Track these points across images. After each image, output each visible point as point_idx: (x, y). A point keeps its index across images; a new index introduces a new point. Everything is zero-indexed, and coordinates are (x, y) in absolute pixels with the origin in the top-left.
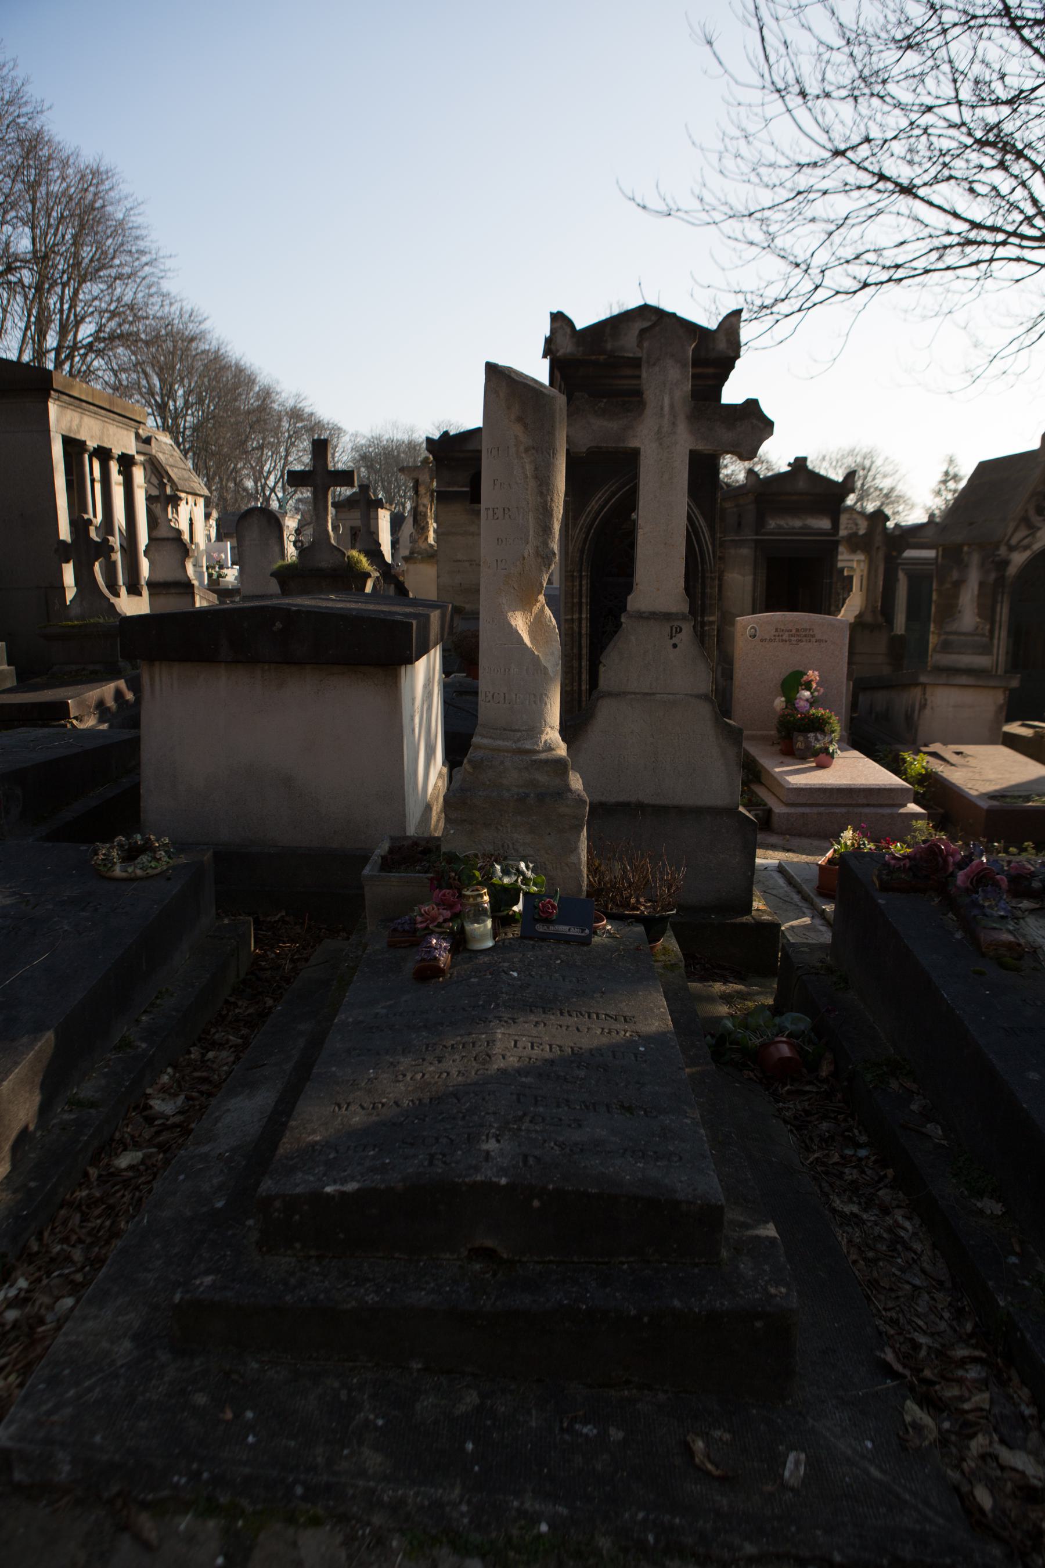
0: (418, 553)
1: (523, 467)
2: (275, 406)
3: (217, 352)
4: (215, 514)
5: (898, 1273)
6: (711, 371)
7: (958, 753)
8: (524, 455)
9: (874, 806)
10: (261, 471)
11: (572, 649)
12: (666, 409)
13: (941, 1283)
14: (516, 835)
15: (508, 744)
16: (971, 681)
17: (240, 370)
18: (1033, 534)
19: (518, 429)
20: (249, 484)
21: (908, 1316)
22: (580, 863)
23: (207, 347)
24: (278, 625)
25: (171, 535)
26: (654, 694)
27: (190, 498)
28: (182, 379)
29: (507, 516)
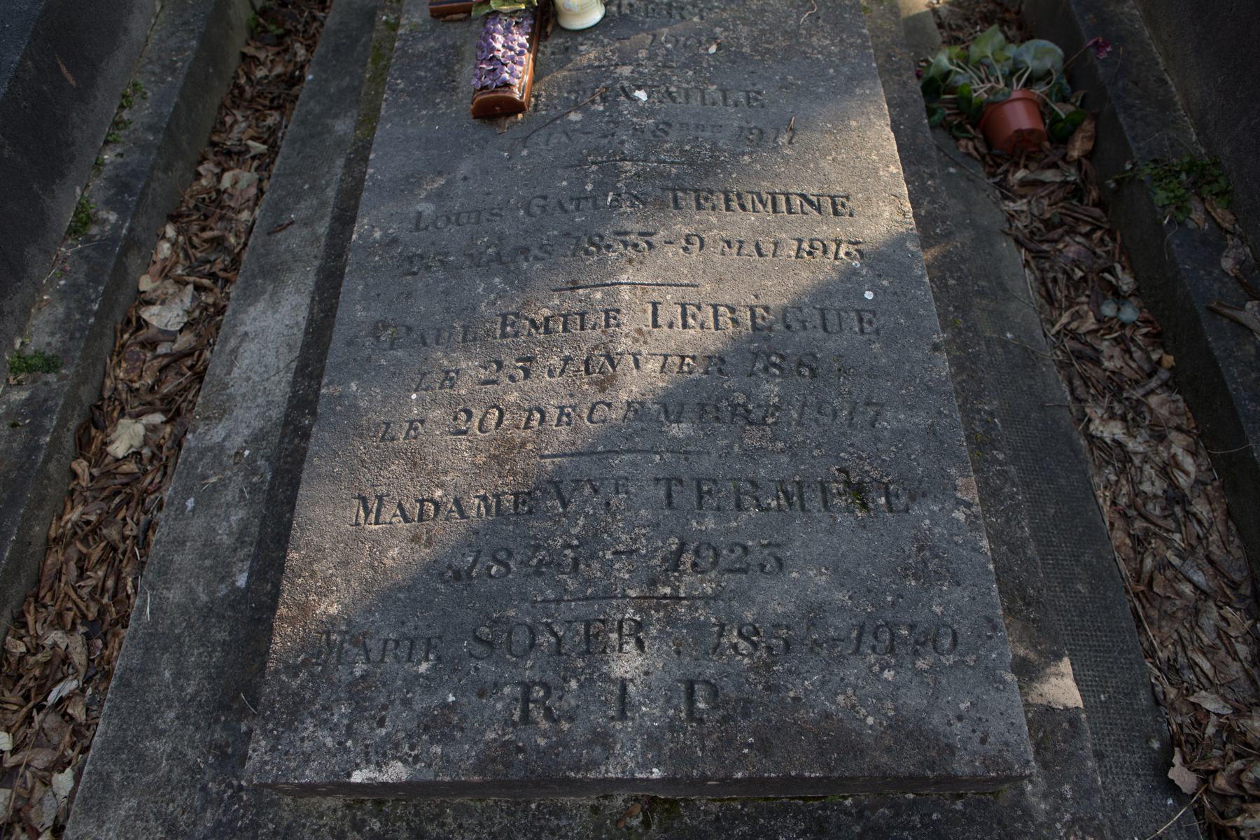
5: (1176, 561)
13: (1234, 586)
21: (1190, 654)
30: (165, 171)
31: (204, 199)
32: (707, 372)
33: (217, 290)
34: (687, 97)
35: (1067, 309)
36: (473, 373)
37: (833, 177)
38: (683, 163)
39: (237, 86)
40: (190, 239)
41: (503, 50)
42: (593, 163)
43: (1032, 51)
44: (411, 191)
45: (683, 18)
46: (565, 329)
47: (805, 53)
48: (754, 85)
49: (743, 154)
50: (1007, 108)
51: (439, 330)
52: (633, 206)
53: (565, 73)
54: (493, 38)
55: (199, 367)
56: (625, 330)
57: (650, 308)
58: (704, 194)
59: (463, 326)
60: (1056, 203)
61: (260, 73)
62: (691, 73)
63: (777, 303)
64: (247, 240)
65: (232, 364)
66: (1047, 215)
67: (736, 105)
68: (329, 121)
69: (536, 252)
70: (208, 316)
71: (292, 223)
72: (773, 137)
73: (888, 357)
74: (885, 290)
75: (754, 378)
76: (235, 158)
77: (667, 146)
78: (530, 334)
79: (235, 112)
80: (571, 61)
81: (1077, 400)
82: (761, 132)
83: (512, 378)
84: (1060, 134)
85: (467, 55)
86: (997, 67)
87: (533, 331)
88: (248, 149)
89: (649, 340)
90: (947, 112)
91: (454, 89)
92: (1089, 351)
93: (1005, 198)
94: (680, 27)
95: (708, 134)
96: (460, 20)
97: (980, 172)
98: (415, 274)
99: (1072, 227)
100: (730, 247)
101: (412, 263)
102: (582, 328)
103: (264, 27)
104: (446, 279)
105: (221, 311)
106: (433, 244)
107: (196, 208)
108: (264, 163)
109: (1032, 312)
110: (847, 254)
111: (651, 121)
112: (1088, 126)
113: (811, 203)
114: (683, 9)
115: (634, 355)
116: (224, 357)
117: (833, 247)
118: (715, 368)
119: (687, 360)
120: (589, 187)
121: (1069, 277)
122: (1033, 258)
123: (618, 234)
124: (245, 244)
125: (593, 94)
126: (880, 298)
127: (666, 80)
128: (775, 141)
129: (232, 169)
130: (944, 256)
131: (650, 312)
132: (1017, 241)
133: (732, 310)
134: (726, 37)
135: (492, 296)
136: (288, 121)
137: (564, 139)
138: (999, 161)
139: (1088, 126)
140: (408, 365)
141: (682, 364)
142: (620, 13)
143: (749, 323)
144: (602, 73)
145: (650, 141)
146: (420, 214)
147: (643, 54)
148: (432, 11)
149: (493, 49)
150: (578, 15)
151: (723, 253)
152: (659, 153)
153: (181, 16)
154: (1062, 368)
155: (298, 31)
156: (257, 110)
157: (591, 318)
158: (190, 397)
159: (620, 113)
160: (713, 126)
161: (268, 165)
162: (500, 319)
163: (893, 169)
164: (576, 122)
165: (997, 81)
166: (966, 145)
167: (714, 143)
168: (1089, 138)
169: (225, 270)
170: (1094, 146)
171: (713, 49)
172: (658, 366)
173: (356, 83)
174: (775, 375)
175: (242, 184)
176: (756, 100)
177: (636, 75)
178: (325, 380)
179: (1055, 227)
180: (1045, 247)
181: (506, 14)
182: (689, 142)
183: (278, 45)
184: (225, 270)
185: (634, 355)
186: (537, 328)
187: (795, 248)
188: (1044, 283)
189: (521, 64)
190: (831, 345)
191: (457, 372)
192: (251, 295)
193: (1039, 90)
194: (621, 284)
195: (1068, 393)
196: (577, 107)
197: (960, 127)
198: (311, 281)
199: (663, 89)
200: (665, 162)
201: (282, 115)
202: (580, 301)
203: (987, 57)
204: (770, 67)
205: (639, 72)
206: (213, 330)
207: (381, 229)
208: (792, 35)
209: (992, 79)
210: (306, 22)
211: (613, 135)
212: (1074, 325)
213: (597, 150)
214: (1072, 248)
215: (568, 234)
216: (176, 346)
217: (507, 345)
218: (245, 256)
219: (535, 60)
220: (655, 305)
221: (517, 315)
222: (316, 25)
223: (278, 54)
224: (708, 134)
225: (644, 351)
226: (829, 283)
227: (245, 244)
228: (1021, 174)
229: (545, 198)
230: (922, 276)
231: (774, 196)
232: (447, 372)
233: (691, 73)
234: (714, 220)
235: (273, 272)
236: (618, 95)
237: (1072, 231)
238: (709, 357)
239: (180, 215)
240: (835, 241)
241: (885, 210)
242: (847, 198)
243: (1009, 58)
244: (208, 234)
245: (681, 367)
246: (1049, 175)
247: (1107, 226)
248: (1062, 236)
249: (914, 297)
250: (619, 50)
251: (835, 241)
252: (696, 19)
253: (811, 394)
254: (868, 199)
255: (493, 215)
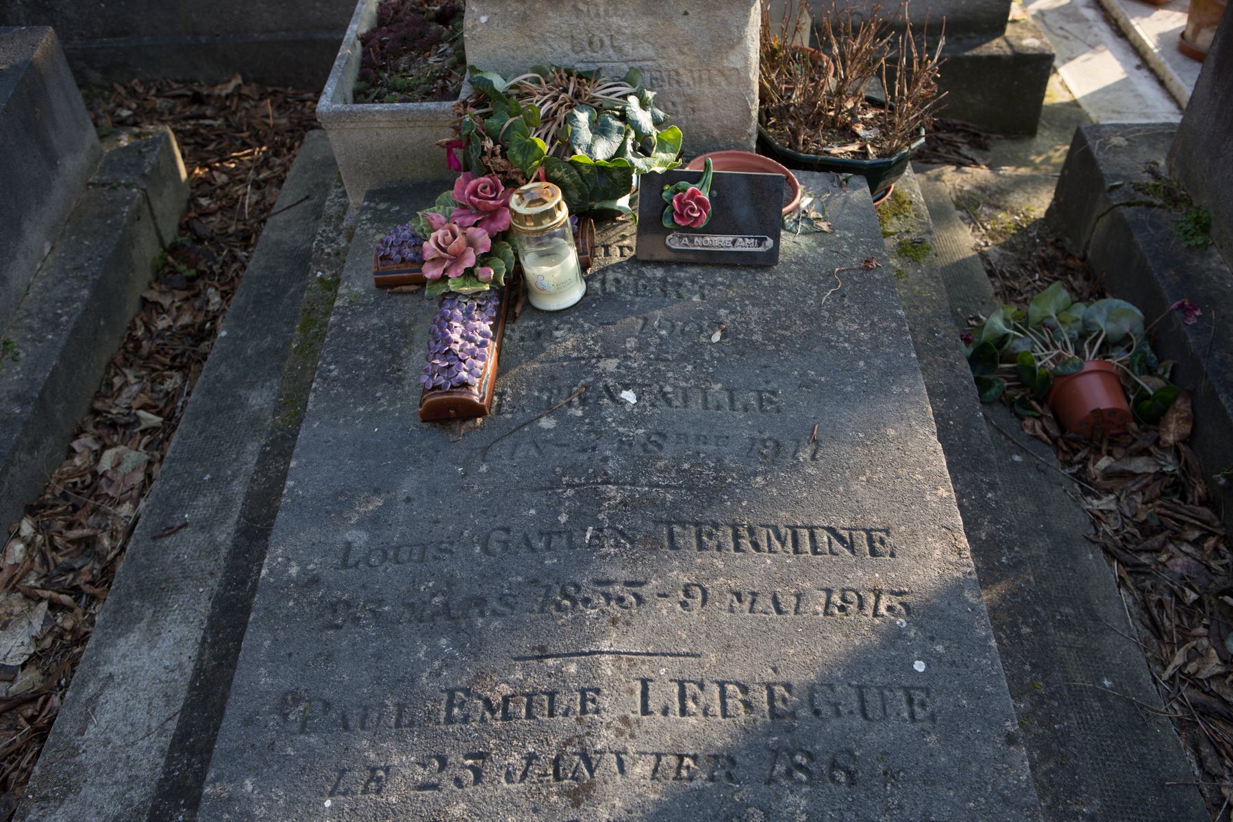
14: (615, 20)
22: (747, 68)
30: (30, 452)
31: (75, 484)
32: (712, 778)
33: (79, 611)
34: (686, 399)
35: (1180, 645)
36: (407, 772)
37: (868, 504)
38: (680, 487)
39: (131, 338)
40: (51, 539)
41: (461, 342)
42: (569, 486)
43: (1105, 311)
44: (340, 513)
45: (680, 296)
46: (529, 715)
47: (828, 341)
48: (767, 382)
49: (756, 474)
50: (1080, 382)
51: (366, 708)
52: (617, 545)
53: (537, 365)
54: (450, 327)
55: (41, 721)
56: (607, 717)
57: (638, 687)
58: (707, 528)
59: (398, 704)
60: (1151, 501)
61: (162, 323)
62: (690, 368)
63: (802, 678)
64: (126, 543)
65: (88, 719)
66: (1143, 517)
67: (746, 410)
68: (242, 392)
69: (495, 604)
70: (62, 646)
71: (185, 525)
72: (791, 450)
73: (949, 754)
74: (940, 658)
75: (773, 786)
76: (121, 431)
77: (661, 464)
78: (483, 720)
79: (127, 371)
80: (543, 349)
81: (1208, 774)
82: (777, 444)
83: (458, 782)
84: (1149, 414)
85: (417, 337)
86: (1064, 329)
87: (488, 715)
88: (138, 420)
89: (637, 732)
90: (1006, 384)
91: (400, 380)
92: (1217, 705)
93: (1087, 493)
94: (676, 309)
95: (711, 448)
96: (411, 293)
97: (1053, 460)
98: (338, 627)
99: (1176, 532)
100: (740, 600)
101: (336, 613)
102: (551, 714)
103: (173, 266)
104: (378, 637)
105: (82, 639)
106: (364, 587)
107: (64, 496)
108: (157, 440)
109: (1134, 649)
110: (890, 609)
111: (640, 431)
112: (1183, 405)
113: (841, 540)
114: (680, 285)
115: (617, 754)
116: (78, 708)
117: (871, 599)
118: (723, 773)
119: (687, 761)
120: (563, 518)
121: (1179, 601)
122: (1129, 573)
123: (599, 583)
124: (123, 549)
125: (570, 394)
126: (934, 670)
127: (659, 376)
128: (794, 456)
129: (115, 445)
130: (1014, 595)
131: (638, 693)
132: (1106, 550)
133: (744, 689)
134: (733, 322)
135: (437, 664)
136: (192, 387)
137: (533, 452)
138: (1075, 446)
139: (1183, 405)
140: (322, 757)
141: (680, 766)
142: (604, 290)
143: (766, 707)
144: (582, 367)
145: (640, 457)
146: (349, 545)
147: (631, 343)
148: (377, 280)
149: (449, 341)
150: (553, 295)
151: (731, 610)
152: (651, 474)
153: (73, 259)
154: (1183, 728)
155: (213, 273)
156: (154, 370)
157: (563, 700)
158: (24, 764)
159: (603, 420)
160: (718, 437)
161: (162, 442)
162: (445, 697)
163: (942, 492)
164: (549, 430)
165: (1065, 347)
166: (1032, 426)
167: (719, 460)
168: (1186, 420)
169: (92, 583)
170: (1192, 431)
171: (716, 337)
172: (648, 770)
173: (280, 345)
174: (800, 782)
175: (126, 466)
176: (771, 402)
177: (623, 371)
178: (211, 775)
179: (1153, 533)
180: (1144, 559)
181: (466, 296)
182: (688, 458)
183: (188, 288)
184: (92, 583)
185: (617, 754)
186: (493, 712)
187: (823, 601)
188: (1147, 609)
189: (483, 358)
190: (872, 737)
191: (387, 770)
192: (122, 622)
193: (1118, 358)
194: (602, 653)
195: (1194, 765)
196: (550, 410)
197: (1023, 402)
198: (204, 607)
199: (656, 388)
200: (658, 486)
201: (185, 378)
202: (550, 675)
203: (1050, 317)
204: (786, 360)
205: (627, 367)
206: (68, 667)
207: (299, 564)
208: (812, 318)
209: (1059, 345)
210: (224, 262)
211: (594, 449)
212: (1191, 668)
213: (574, 469)
214: (1179, 560)
215: (535, 582)
216: (14, 687)
217: (454, 735)
218: (120, 567)
219: (499, 350)
220: (645, 682)
221: (467, 692)
222: (235, 266)
223: (187, 299)
224: (711, 448)
225: (631, 749)
226: (867, 650)
227: (123, 549)
228: (1104, 462)
229: (507, 530)
230: (987, 638)
231: (794, 530)
232: (374, 770)
233: (690, 368)
234: (719, 564)
235: (155, 592)
236: (601, 397)
237: (1176, 538)
238: (715, 757)
239: (43, 506)
240: (874, 591)
241: (935, 552)
242: (887, 532)
243: (1076, 320)
244: (75, 533)
245: (678, 772)
246: (1140, 465)
247: (1221, 532)
248: (1164, 544)
249: (978, 668)
250: (603, 338)
251: (874, 591)
252: (696, 299)
253: (849, 809)
254: (913, 532)
255: (441, 550)
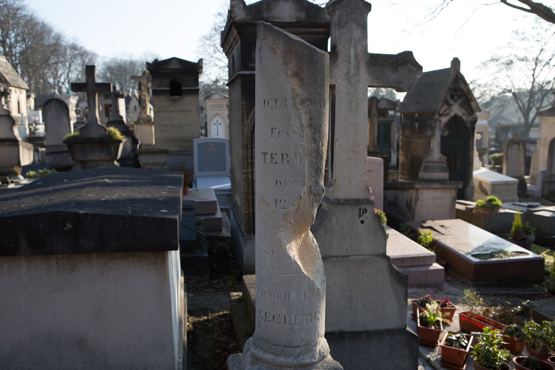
0: (142, 120)
1: (300, 117)
2: (63, 43)
3: (31, 16)
4: (33, 96)
6: (322, 30)
7: (442, 226)
8: (300, 107)
9: (416, 266)
10: (57, 74)
11: (248, 189)
12: (352, 58)
15: (290, 360)
16: (440, 186)
17: (44, 26)
18: (450, 108)
19: (294, 83)
20: (51, 80)
23: (26, 13)
24: (69, 226)
25: (4, 113)
26: (349, 256)
27: (18, 90)
28: (13, 29)
29: (285, 161)
